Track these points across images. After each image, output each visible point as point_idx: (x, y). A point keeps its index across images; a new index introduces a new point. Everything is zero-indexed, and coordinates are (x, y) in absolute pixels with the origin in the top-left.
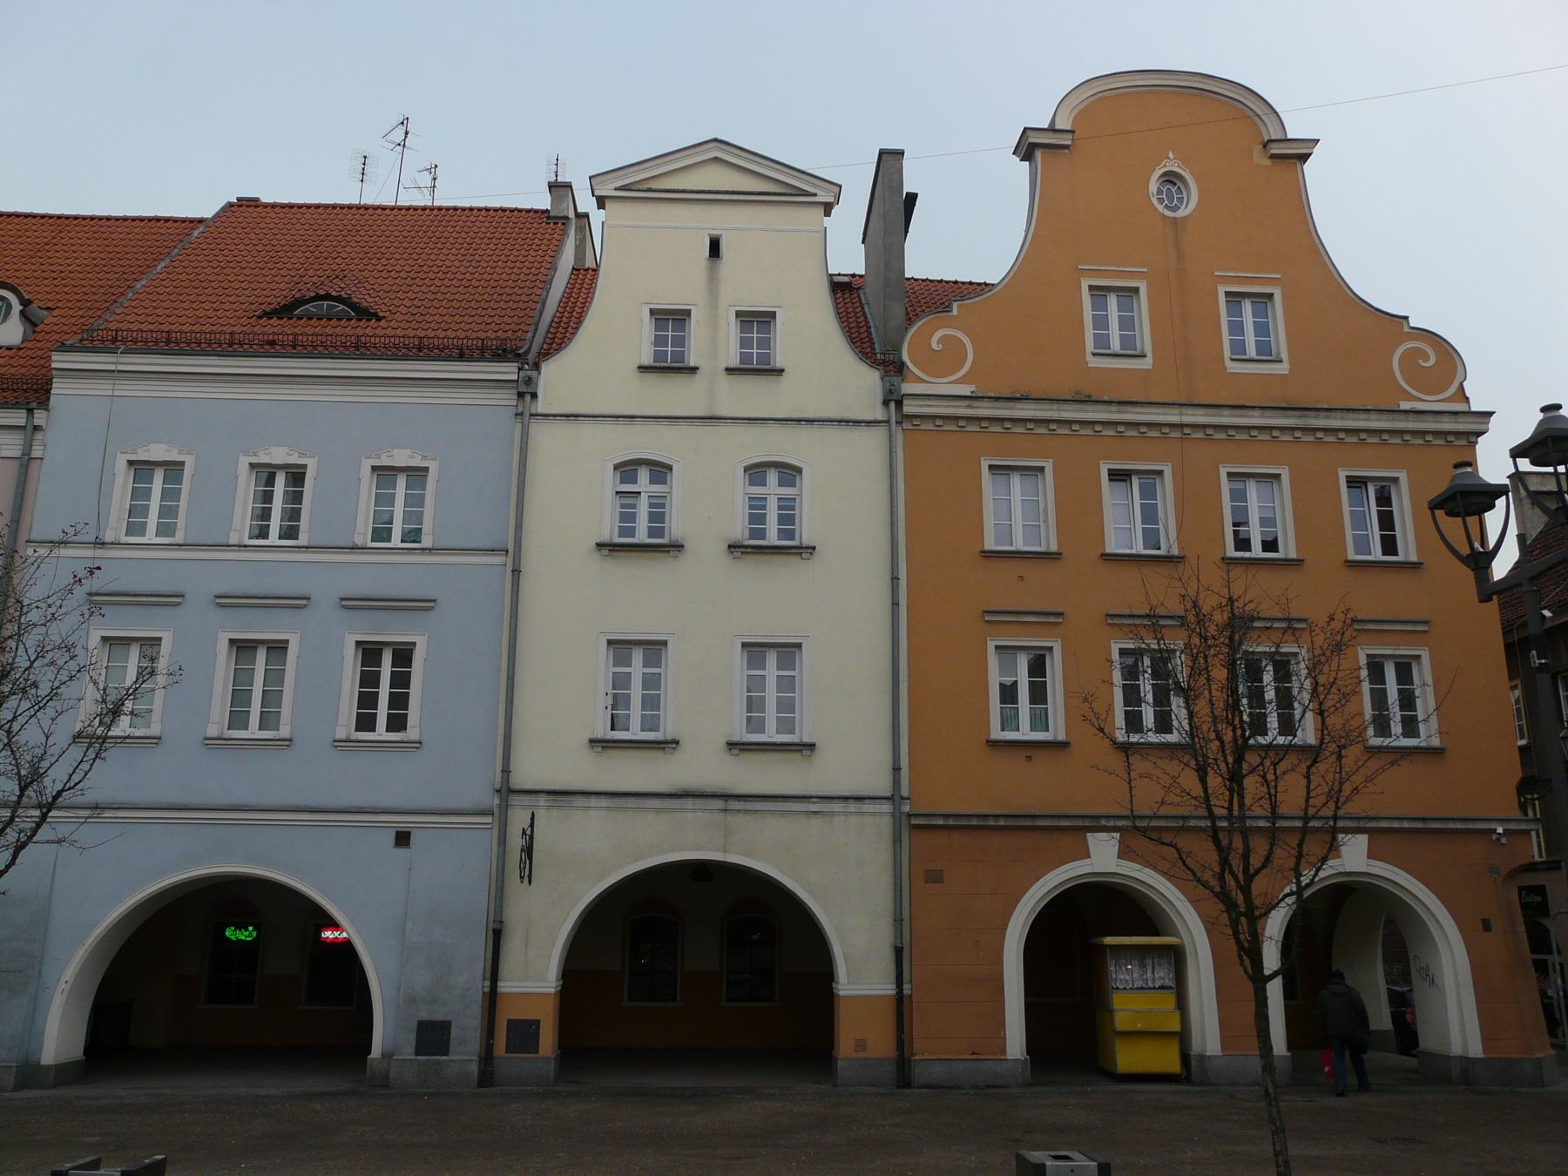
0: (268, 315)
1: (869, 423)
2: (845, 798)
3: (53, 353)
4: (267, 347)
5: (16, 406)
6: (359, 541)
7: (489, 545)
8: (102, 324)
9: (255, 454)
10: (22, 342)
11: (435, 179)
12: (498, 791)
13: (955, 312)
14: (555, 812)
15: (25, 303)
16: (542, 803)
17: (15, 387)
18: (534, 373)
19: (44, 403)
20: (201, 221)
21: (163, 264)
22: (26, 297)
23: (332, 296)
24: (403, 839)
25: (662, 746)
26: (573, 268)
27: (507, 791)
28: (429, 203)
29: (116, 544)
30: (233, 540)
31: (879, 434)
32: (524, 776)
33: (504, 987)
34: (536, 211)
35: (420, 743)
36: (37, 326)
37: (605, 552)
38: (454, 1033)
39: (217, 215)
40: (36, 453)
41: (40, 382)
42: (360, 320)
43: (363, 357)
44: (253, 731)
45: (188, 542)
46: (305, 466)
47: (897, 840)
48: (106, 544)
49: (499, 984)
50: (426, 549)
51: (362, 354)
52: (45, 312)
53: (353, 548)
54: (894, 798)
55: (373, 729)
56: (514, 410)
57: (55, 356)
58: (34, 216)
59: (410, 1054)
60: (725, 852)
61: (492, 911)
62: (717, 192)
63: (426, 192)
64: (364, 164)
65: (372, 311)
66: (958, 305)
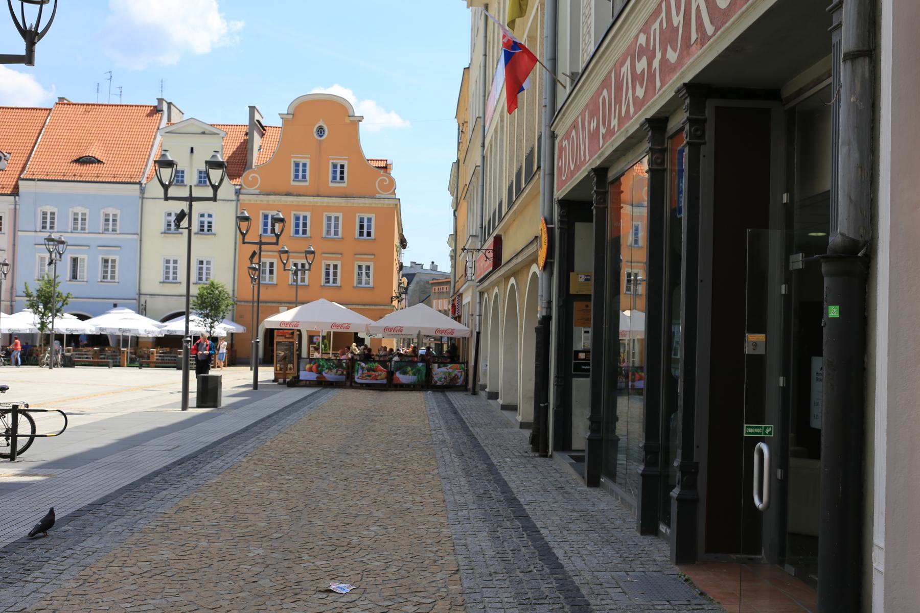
27: (140, 294)
44: (363, 285)
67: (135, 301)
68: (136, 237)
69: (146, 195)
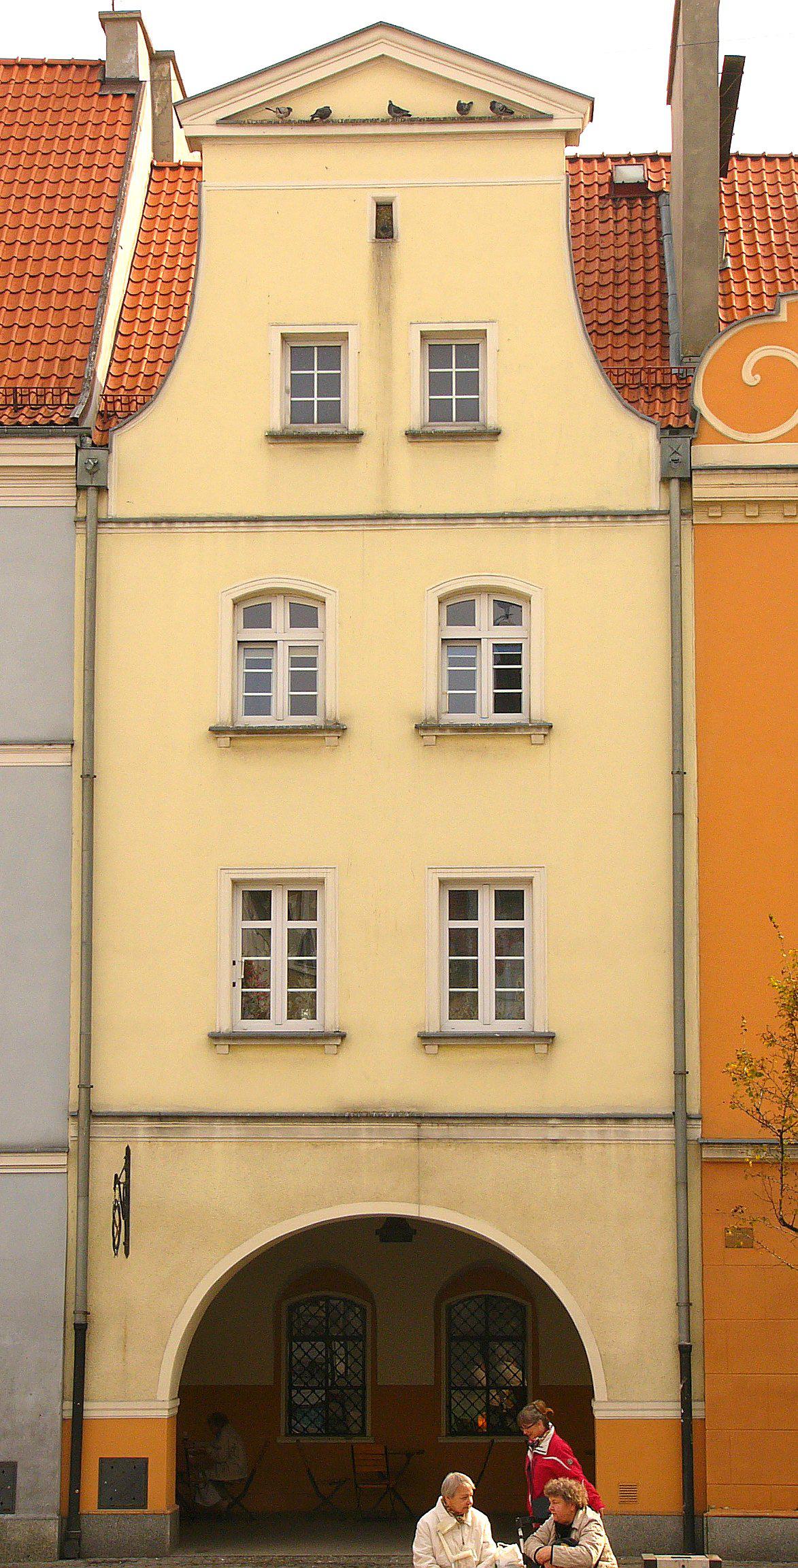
1: (637, 515)
2: (601, 1119)
13: (783, 317)
14: (161, 1147)
16: (141, 1134)
25: (320, 1042)
31: (654, 535)
32: (110, 1095)
33: (93, 1409)
37: (225, 740)
47: (682, 1183)
49: (86, 1405)
54: (679, 1117)
60: (419, 1202)
62: (364, 122)
66: (788, 304)
67: (61, 1159)
68: (57, 757)
69: (115, 506)
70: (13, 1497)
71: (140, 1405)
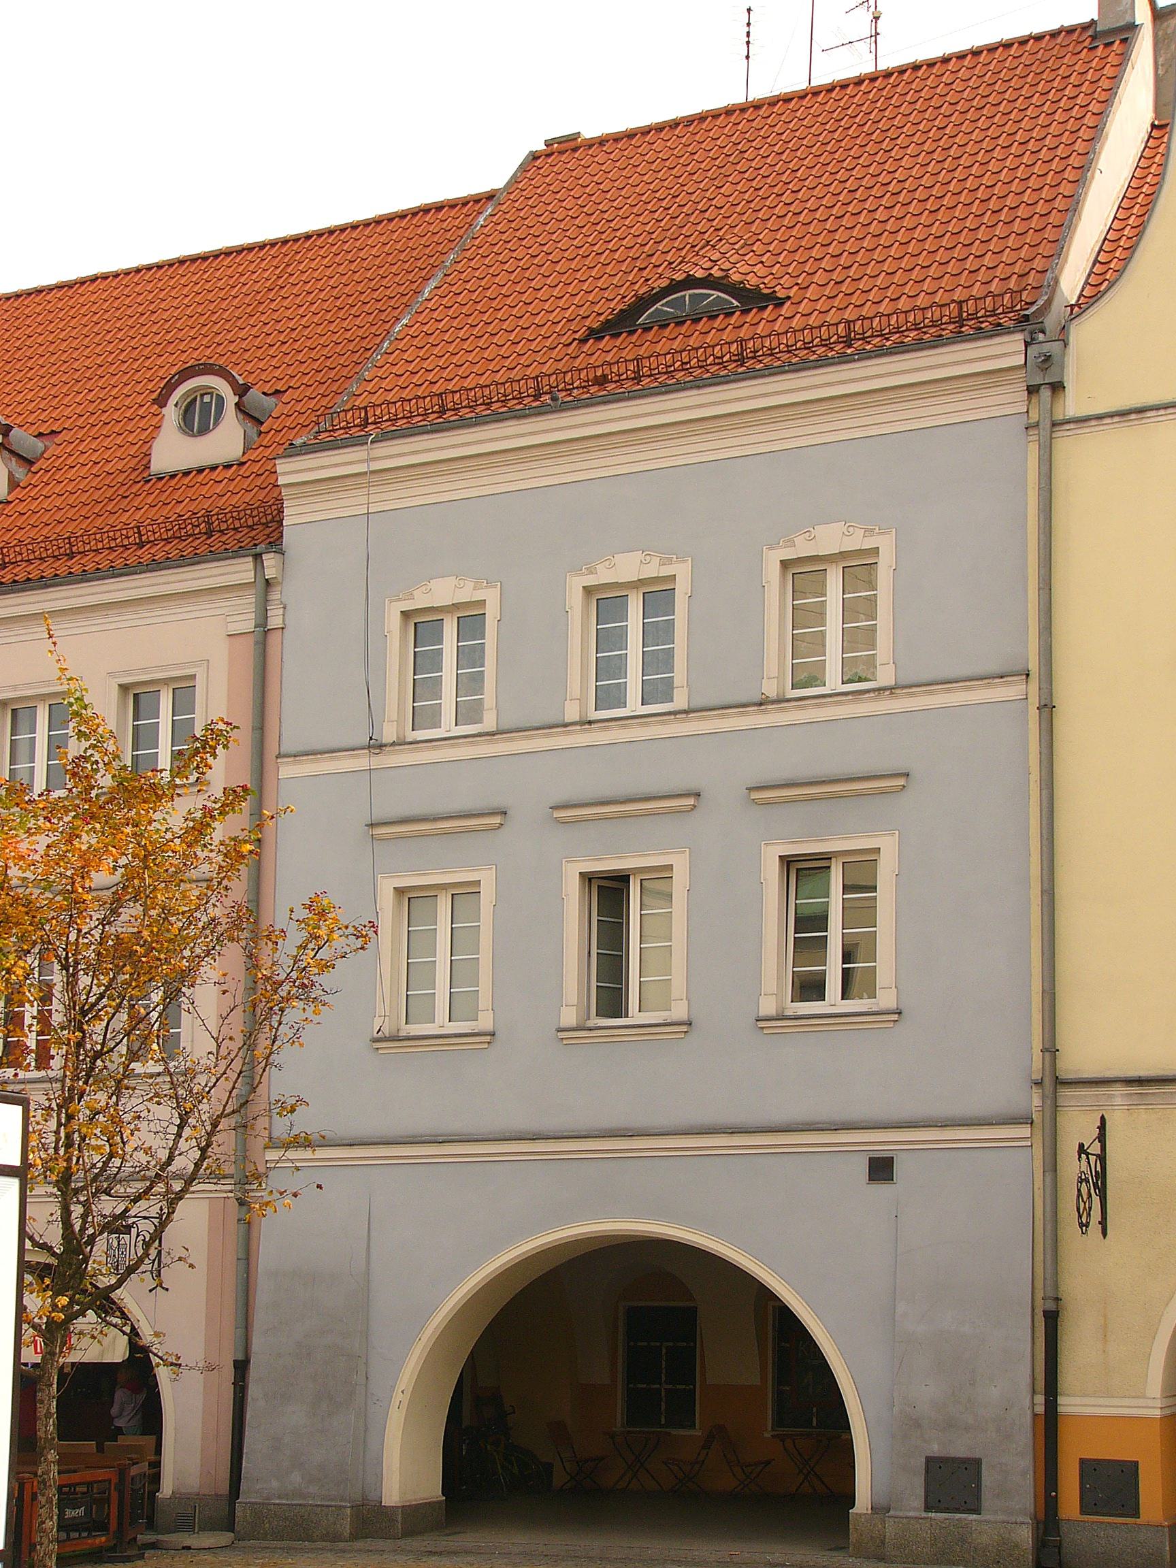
0: (595, 334)
3: (277, 462)
4: (593, 389)
5: (238, 553)
6: (770, 690)
7: (994, 667)
8: (347, 401)
9: (591, 571)
10: (244, 453)
11: (877, 18)
12: (1038, 1084)
14: (1143, 1115)
15: (241, 391)
16: (1118, 1101)
17: (224, 526)
18: (1055, 348)
19: (275, 542)
20: (490, 196)
21: (433, 284)
22: (241, 382)
23: (697, 279)
24: (881, 1169)
26: (1153, 126)
28: (869, 68)
29: (401, 743)
30: (572, 714)
33: (1068, 1405)
34: (1070, 31)
35: (900, 1013)
36: (262, 423)
38: (988, 1478)
39: (514, 180)
40: (275, 621)
41: (255, 513)
42: (745, 312)
43: (752, 375)
45: (505, 726)
46: (673, 578)
48: (385, 746)
50: (885, 689)
51: (767, 368)
52: (272, 400)
53: (761, 704)
55: (821, 997)
56: (1024, 420)
57: (282, 466)
58: (250, 248)
59: (915, 1509)
61: (1039, 1284)
63: (863, 47)
64: (749, 24)
65: (766, 291)
69: (1073, 404)
70: (979, 1498)
71: (1126, 1402)
